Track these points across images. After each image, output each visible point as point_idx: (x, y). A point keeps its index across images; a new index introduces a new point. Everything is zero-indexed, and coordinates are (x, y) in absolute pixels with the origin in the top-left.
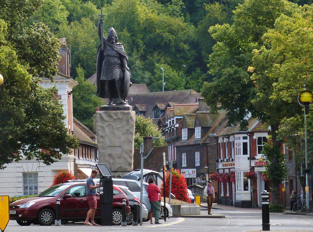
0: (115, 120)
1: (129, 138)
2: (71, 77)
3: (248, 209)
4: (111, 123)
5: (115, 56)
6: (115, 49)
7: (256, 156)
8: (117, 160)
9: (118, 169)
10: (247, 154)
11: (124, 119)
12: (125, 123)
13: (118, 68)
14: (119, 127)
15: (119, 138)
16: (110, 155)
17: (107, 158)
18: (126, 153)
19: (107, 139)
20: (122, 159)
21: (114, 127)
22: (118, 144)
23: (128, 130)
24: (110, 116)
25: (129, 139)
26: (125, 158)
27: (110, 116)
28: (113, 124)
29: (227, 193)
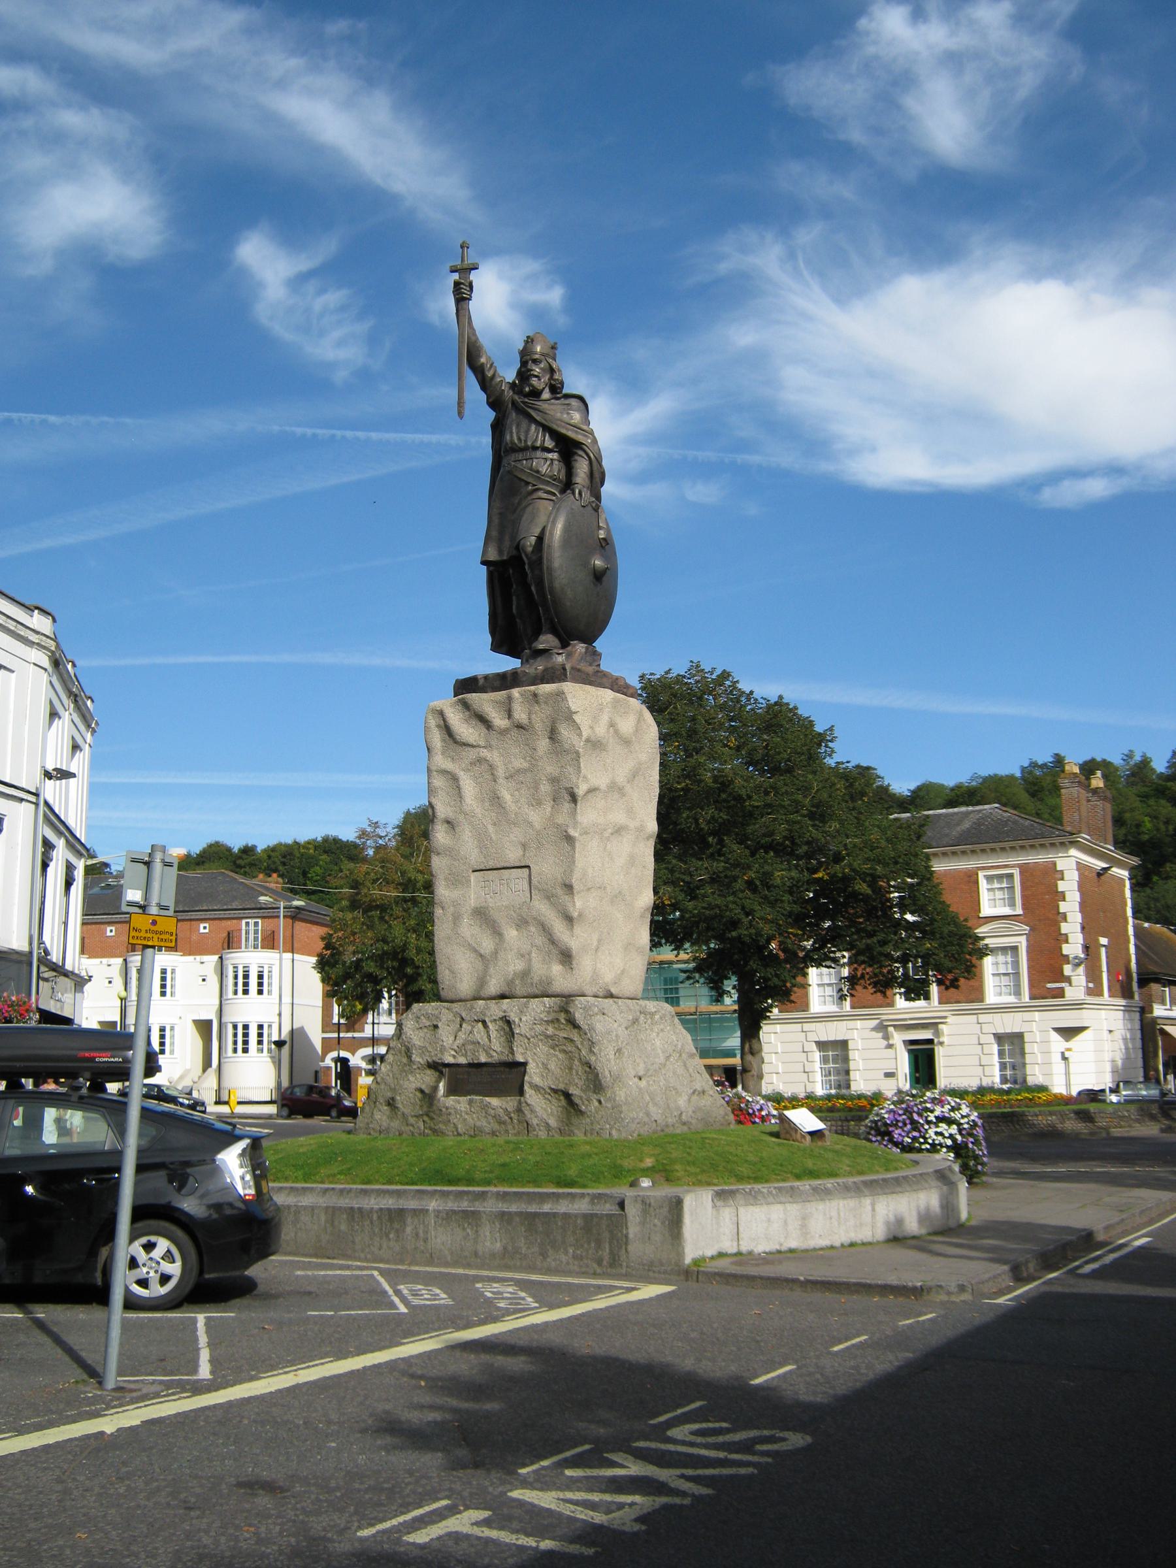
0: (503, 732)
1: (561, 819)
2: (508, 664)
3: (918, 489)
4: (484, 753)
5: (538, 444)
6: (538, 418)
7: (1145, 763)
8: (511, 933)
9: (510, 983)
10: (1062, 989)
13: (545, 496)
14: (518, 771)
18: (549, 897)
19: (467, 834)
20: (533, 929)
21: (501, 772)
22: (513, 855)
24: (484, 721)
25: (558, 826)
27: (484, 721)
28: (494, 756)
29: (102, 1433)
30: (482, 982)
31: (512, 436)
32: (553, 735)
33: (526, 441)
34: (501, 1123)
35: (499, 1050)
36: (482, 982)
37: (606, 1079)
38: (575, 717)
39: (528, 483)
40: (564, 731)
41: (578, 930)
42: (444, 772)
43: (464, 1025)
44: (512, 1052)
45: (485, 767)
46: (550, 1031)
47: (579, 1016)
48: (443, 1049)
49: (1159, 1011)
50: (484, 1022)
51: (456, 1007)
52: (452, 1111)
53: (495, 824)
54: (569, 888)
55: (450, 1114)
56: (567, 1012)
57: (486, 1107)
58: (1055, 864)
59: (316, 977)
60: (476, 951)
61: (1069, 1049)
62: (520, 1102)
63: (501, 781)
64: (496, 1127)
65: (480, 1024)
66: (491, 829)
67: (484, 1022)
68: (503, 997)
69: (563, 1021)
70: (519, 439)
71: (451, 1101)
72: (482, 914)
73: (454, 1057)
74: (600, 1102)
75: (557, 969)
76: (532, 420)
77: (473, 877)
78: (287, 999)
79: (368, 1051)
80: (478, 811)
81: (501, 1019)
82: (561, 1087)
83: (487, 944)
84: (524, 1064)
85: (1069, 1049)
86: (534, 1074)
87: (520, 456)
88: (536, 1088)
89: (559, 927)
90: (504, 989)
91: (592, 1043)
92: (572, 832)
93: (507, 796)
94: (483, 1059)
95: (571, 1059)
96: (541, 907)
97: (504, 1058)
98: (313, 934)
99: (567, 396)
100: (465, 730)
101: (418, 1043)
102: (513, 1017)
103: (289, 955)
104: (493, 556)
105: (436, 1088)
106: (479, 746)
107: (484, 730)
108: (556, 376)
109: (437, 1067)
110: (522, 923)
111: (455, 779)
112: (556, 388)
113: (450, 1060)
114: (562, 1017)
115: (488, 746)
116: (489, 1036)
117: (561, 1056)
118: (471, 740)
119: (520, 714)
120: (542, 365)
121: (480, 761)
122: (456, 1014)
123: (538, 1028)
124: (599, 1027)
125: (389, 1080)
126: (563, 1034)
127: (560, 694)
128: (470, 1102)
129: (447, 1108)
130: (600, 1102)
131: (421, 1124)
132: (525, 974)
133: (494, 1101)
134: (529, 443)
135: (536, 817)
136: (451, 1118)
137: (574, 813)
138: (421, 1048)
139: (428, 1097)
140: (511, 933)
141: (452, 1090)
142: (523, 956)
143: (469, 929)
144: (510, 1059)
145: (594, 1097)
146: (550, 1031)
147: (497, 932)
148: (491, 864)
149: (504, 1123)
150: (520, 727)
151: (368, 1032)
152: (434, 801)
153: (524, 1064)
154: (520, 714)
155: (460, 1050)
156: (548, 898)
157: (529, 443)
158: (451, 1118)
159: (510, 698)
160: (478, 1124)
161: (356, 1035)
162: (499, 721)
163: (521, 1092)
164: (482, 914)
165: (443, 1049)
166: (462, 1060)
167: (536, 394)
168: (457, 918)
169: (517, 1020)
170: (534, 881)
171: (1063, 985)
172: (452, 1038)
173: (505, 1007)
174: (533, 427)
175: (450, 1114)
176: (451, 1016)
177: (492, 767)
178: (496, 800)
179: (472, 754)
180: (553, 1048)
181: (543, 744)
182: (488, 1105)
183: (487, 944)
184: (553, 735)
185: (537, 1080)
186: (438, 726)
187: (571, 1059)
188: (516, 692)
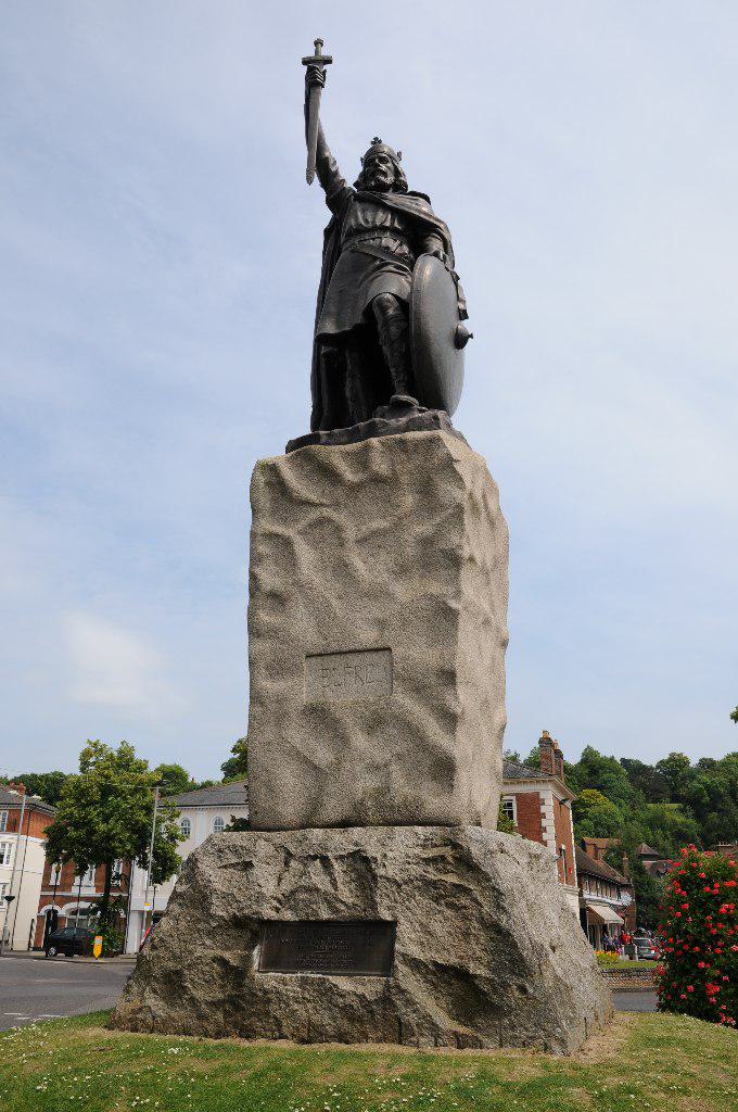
4: (327, 512)
5: (388, 224)
8: (359, 740)
11: (405, 479)
12: (409, 500)
15: (378, 594)
16: (318, 715)
17: (297, 735)
21: (351, 534)
22: (368, 636)
23: (426, 542)
26: (409, 725)
28: (340, 517)
30: (315, 804)
31: (356, 218)
33: (374, 222)
34: (352, 1019)
35: (350, 901)
36: (315, 804)
38: (457, 467)
39: (375, 258)
41: (460, 732)
43: (293, 863)
44: (374, 906)
45: (328, 529)
49: (586, 896)
50: (325, 861)
51: (278, 837)
52: (272, 996)
53: (340, 598)
55: (269, 1001)
57: (327, 993)
58: (538, 794)
59: (43, 852)
60: (306, 761)
62: (387, 986)
63: (350, 544)
64: (346, 1025)
65: (318, 862)
66: (334, 602)
67: (325, 861)
69: (450, 859)
70: (367, 221)
71: (270, 979)
73: (277, 910)
74: (523, 990)
78: (19, 867)
79: (73, 905)
80: (317, 580)
81: (352, 855)
84: (394, 924)
86: (408, 941)
88: (415, 964)
89: (434, 731)
91: (498, 894)
93: (358, 564)
94: (325, 915)
98: (39, 825)
99: (414, 194)
101: (217, 886)
102: (372, 851)
103: (25, 837)
104: (330, 328)
105: (247, 960)
106: (322, 505)
108: (402, 178)
109: (248, 927)
110: (375, 723)
111: (287, 543)
112: (399, 187)
115: (336, 505)
116: (334, 883)
117: (449, 913)
118: (313, 498)
119: (381, 465)
120: (390, 165)
122: (278, 847)
125: (175, 945)
127: (434, 442)
128: (304, 982)
129: (266, 992)
130: (523, 990)
131: (220, 1016)
133: (343, 983)
134: (378, 224)
135: (402, 591)
136: (272, 1007)
138: (225, 896)
139: (235, 975)
140: (359, 740)
141: (270, 964)
142: (377, 768)
144: (370, 915)
145: (514, 981)
146: (433, 875)
147: (341, 739)
148: (335, 647)
149: (360, 1020)
150: (377, 480)
151: (75, 891)
154: (381, 465)
155: (288, 899)
156: (417, 690)
157: (378, 224)
158: (272, 1007)
159: (367, 448)
160: (315, 1018)
161: (65, 894)
162: (350, 476)
163: (387, 968)
165: (260, 898)
166: (288, 916)
167: (384, 188)
169: (379, 856)
172: (275, 882)
173: (355, 838)
175: (269, 1001)
176: (271, 850)
177: (338, 529)
178: (342, 569)
179: (314, 515)
180: (437, 901)
182: (333, 989)
183: (323, 755)
185: (415, 951)
188: (374, 441)
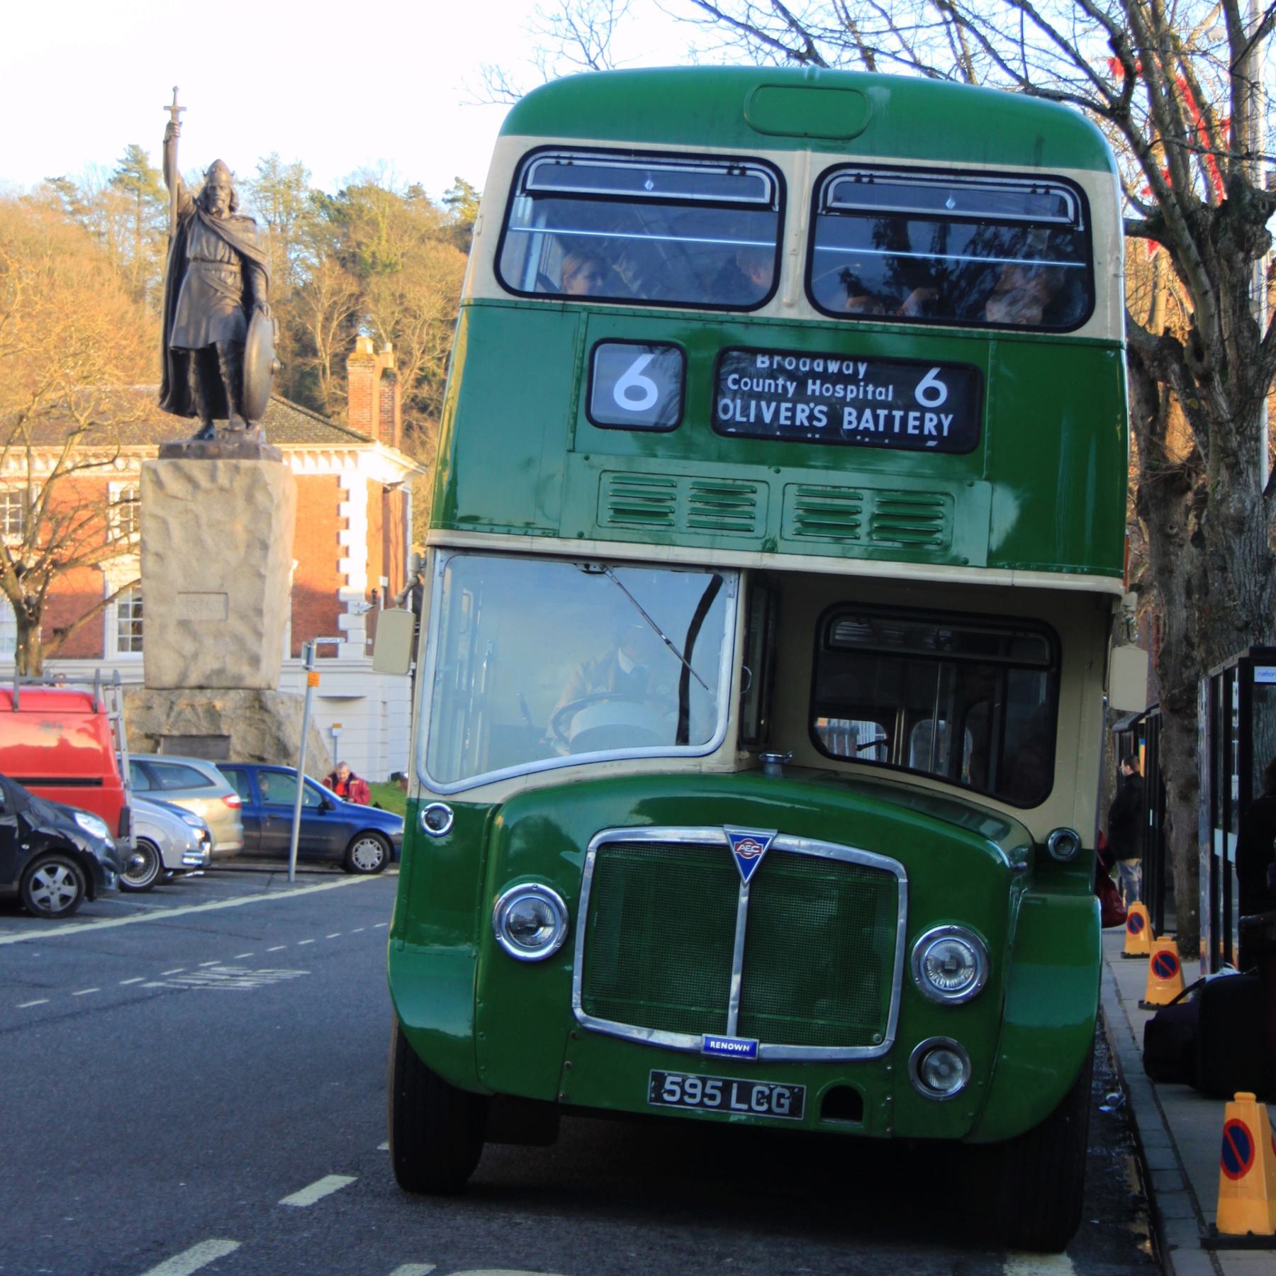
4: (191, 506)
8: (209, 642)
9: (209, 677)
10: (335, 646)
18: (243, 617)
21: (204, 520)
22: (213, 584)
24: (190, 480)
27: (190, 480)
32: (250, 498)
36: (184, 675)
37: (291, 749)
40: (260, 497)
42: (155, 517)
46: (248, 713)
47: (270, 704)
48: (160, 725)
54: (259, 612)
56: (260, 701)
61: (338, 726)
68: (201, 688)
72: (184, 624)
75: (245, 669)
76: (220, 238)
77: (179, 598)
82: (257, 753)
83: (189, 647)
85: (338, 726)
87: (210, 266)
90: (203, 682)
92: (263, 571)
94: (194, 732)
95: (263, 734)
96: (236, 625)
97: (212, 732)
100: (174, 485)
107: (190, 488)
110: (218, 635)
113: (165, 732)
114: (257, 704)
118: (180, 495)
121: (187, 511)
123: (239, 712)
124: (282, 712)
126: (257, 717)
132: (220, 672)
137: (265, 557)
140: (209, 642)
143: (173, 635)
144: (217, 733)
148: (194, 589)
150: (222, 489)
152: (146, 538)
153: (227, 738)
154: (223, 479)
162: (204, 482)
164: (184, 624)
165: (160, 725)
168: (163, 627)
170: (231, 604)
171: (338, 640)
174: (221, 244)
177: (197, 517)
178: (199, 542)
181: (240, 503)
184: (250, 498)
185: (239, 748)
186: (152, 481)
187: (263, 734)
